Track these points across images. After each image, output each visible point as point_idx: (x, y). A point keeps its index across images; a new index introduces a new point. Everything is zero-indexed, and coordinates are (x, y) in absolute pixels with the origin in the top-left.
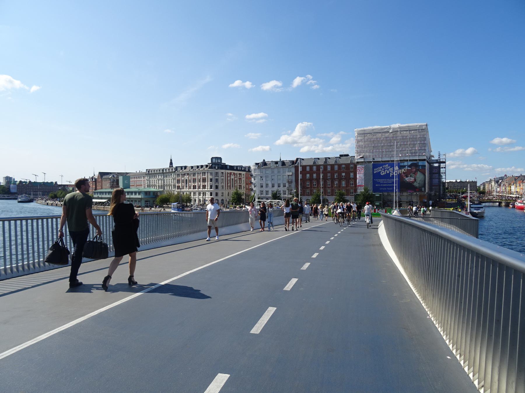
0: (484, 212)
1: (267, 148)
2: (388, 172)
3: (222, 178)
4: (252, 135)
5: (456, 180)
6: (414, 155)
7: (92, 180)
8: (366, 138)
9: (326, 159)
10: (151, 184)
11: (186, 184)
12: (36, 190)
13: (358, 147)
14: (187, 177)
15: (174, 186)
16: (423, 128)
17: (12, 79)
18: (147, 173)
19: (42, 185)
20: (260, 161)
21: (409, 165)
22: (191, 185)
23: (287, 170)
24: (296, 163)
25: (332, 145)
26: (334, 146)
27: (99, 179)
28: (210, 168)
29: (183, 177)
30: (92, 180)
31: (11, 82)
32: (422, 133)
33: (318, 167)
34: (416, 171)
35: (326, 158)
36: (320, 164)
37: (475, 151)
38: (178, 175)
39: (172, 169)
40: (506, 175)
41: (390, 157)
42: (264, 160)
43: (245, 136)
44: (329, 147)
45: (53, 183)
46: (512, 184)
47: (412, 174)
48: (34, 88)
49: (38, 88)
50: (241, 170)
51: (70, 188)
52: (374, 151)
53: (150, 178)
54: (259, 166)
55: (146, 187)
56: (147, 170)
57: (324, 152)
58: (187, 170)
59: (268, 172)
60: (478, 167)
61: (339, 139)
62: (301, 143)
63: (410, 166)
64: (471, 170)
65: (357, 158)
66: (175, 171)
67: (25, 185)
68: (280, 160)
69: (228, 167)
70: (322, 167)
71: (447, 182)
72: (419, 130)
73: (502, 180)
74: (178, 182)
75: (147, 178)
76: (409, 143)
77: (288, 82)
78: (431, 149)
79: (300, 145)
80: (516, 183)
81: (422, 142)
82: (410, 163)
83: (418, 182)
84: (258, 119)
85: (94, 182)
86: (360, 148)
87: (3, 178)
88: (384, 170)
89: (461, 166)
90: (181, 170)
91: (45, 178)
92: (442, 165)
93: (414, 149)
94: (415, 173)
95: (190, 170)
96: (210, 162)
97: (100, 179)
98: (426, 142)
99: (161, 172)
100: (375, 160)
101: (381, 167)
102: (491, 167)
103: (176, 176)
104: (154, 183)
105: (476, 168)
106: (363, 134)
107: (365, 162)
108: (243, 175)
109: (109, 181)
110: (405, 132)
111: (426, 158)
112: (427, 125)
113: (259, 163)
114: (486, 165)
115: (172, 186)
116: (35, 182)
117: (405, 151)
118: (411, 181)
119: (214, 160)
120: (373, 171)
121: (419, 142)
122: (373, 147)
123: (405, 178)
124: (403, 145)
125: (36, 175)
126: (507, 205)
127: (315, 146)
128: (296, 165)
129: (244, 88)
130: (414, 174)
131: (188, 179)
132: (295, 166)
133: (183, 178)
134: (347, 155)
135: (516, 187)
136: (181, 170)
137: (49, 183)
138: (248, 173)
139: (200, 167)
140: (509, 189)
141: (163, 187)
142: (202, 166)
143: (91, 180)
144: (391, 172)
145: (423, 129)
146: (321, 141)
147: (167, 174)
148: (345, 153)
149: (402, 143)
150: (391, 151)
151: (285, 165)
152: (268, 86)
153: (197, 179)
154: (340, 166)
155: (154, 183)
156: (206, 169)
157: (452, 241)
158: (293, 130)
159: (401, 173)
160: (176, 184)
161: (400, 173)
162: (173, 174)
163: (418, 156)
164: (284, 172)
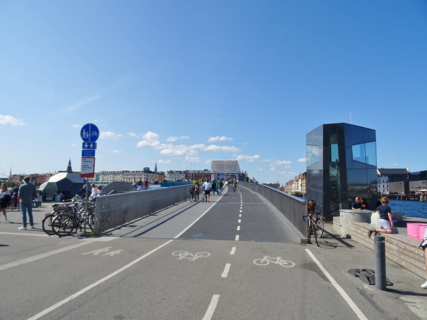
3: (150, 177)
6: (232, 171)
10: (115, 179)
11: (129, 179)
13: (212, 167)
18: (102, 173)
20: (169, 170)
23: (182, 175)
28: (144, 172)
33: (196, 174)
34: (233, 178)
35: (199, 171)
36: (196, 173)
42: (171, 170)
65: (212, 172)
66: (122, 173)
69: (152, 173)
70: (197, 174)
82: (231, 174)
103: (123, 175)
110: (229, 163)
119: (146, 169)
121: (234, 167)
128: (186, 173)
131: (130, 177)
134: (207, 170)
139: (138, 172)
142: (139, 172)
148: (207, 169)
153: (136, 177)
154: (204, 174)
164: (181, 176)
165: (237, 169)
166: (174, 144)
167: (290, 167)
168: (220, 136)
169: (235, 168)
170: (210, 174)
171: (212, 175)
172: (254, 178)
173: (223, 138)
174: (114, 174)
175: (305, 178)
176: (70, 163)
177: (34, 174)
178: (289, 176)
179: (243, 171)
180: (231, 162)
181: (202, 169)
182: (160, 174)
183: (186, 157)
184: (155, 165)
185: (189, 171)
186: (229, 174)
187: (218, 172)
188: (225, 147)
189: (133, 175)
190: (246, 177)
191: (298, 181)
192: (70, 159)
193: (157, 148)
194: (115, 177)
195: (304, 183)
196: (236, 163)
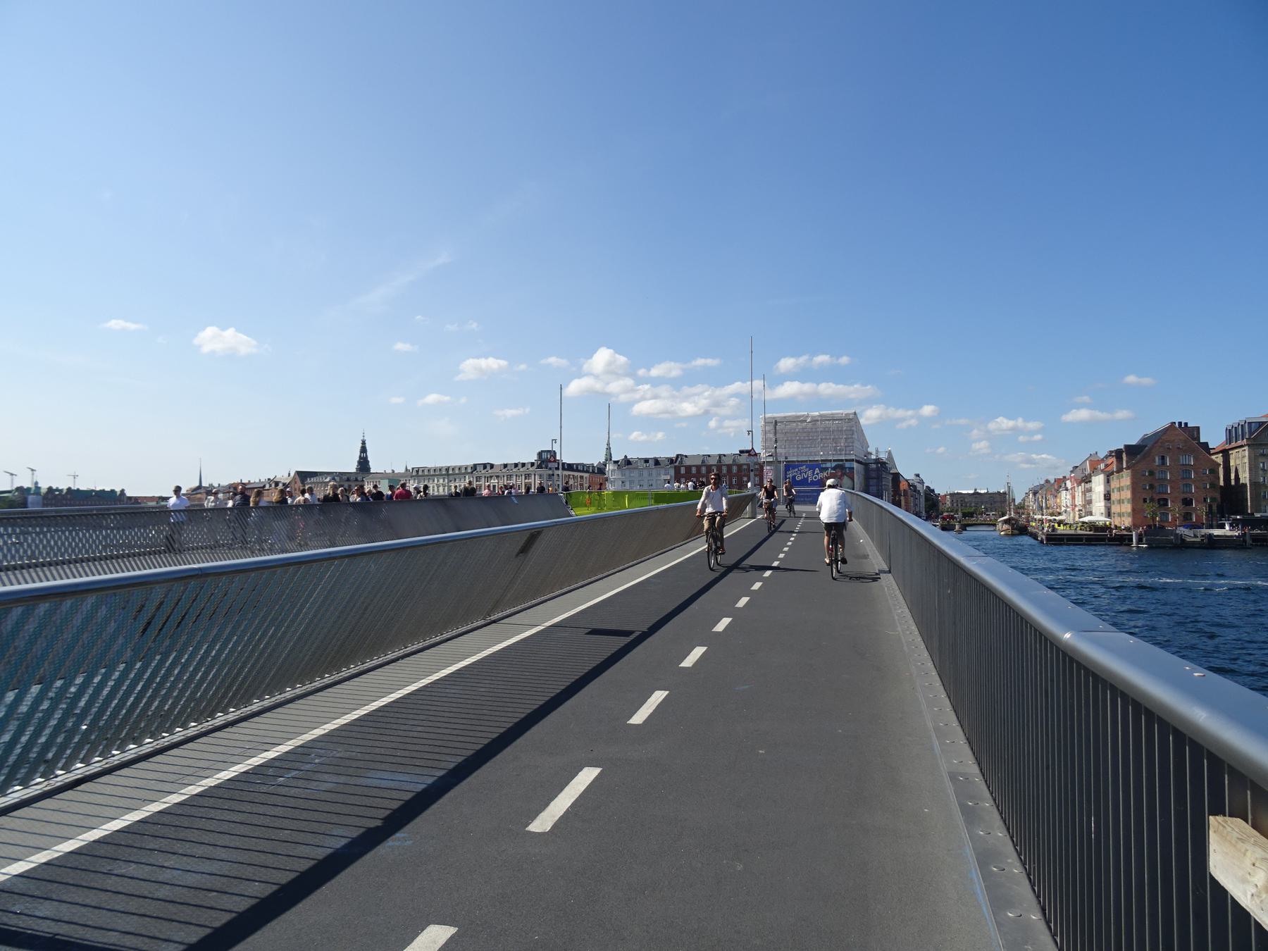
2: (806, 477)
5: (976, 490)
6: (839, 453)
9: (720, 457)
18: (414, 473)
23: (663, 471)
24: (676, 462)
27: (296, 483)
28: (538, 467)
33: (709, 469)
34: (843, 475)
35: (720, 456)
42: (626, 456)
48: (463, 400)
50: (583, 471)
52: (787, 446)
66: (472, 472)
67: (59, 497)
82: (834, 464)
88: (801, 474)
99: (463, 471)
100: (788, 460)
101: (796, 470)
110: (827, 422)
119: (544, 456)
128: (677, 464)
132: (675, 467)
139: (520, 466)
142: (523, 465)
143: (273, 485)
149: (824, 437)
154: (740, 466)
157: (1128, 696)
162: (467, 477)
165: (857, 444)
166: (676, 384)
167: (1038, 437)
168: (815, 354)
169: (849, 441)
170: (760, 464)
171: (766, 468)
172: (918, 475)
173: (822, 359)
174: (448, 475)
175: (1128, 468)
176: (364, 450)
177: (238, 484)
178: (1033, 466)
179: (877, 451)
180: (833, 418)
181: (730, 448)
182: (593, 472)
183: (712, 419)
184: (606, 446)
185: (686, 456)
186: (828, 465)
187: (786, 458)
188: (831, 384)
189: (523, 477)
190: (891, 472)
191: (1087, 480)
192: (365, 438)
193: (623, 398)
194: (451, 486)
195: (1120, 489)
196: (853, 423)
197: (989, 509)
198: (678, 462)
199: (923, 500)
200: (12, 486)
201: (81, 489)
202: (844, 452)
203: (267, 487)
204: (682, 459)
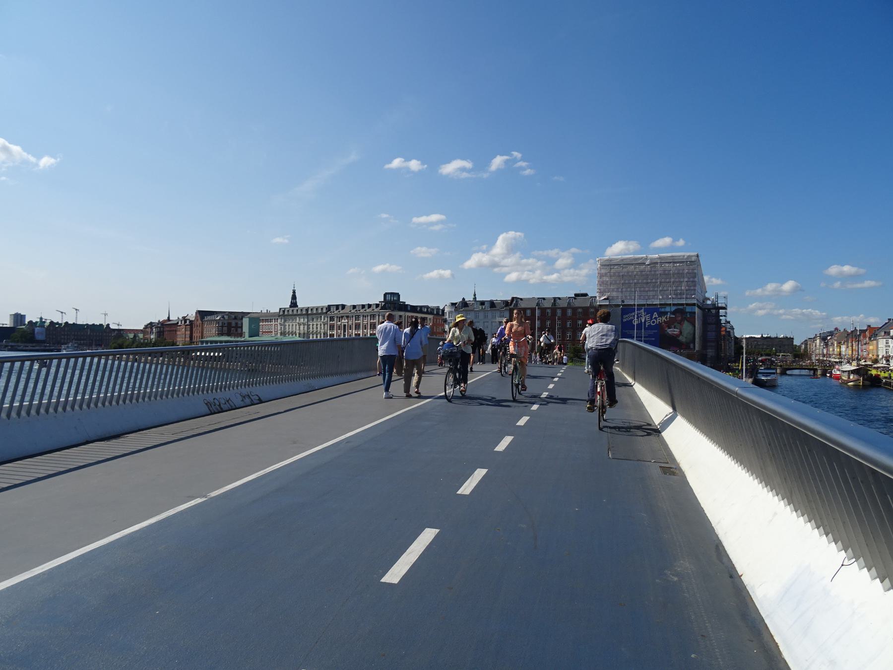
0: (775, 380)
1: (447, 273)
4: (422, 252)
5: (762, 335)
6: (679, 296)
7: (185, 322)
8: (612, 271)
9: (555, 301)
11: (345, 331)
12: (85, 337)
13: (601, 283)
14: (346, 321)
15: (324, 334)
16: (693, 260)
17: (7, 144)
18: (281, 313)
19: (85, 329)
20: (458, 300)
21: (672, 311)
22: (352, 333)
23: (498, 314)
24: (511, 305)
25: (558, 271)
26: (560, 274)
27: (197, 321)
29: (339, 322)
30: (185, 322)
31: (5, 149)
32: (691, 266)
33: (543, 310)
35: (555, 299)
37: (797, 287)
38: (332, 319)
39: (297, 310)
40: (836, 329)
41: (647, 299)
42: (464, 299)
43: (412, 252)
44: (553, 274)
45: (103, 326)
46: (843, 342)
47: (676, 324)
49: (52, 161)
50: (427, 313)
51: (129, 335)
52: (624, 290)
53: (285, 321)
54: (456, 307)
55: (279, 334)
56: (280, 309)
57: (544, 283)
58: (346, 310)
59: (470, 316)
60: (803, 314)
61: (569, 261)
62: (506, 266)
63: (673, 313)
64: (792, 318)
65: (600, 300)
66: (326, 313)
67: (59, 329)
68: (475, 298)
69: (409, 309)
70: (549, 311)
71: (746, 338)
72: (687, 262)
73: (832, 336)
74: (331, 329)
75: (281, 321)
76: (672, 280)
77: (481, 163)
78: (706, 289)
79: (506, 269)
80: (847, 341)
81: (691, 279)
82: (673, 308)
83: (685, 336)
84: (432, 224)
85: (189, 327)
86: (603, 287)
87: (9, 316)
89: (775, 312)
90: (336, 310)
91: (76, 318)
92: (722, 312)
93: (680, 288)
94: (681, 323)
95: (350, 311)
96: (383, 300)
97: (200, 321)
98: (696, 279)
99: (320, 311)
100: (625, 303)
102: (824, 314)
104: (317, 328)
105: (799, 316)
106: (608, 265)
107: (611, 305)
108: (430, 319)
109: (216, 325)
110: (667, 265)
111: (696, 302)
112: (698, 256)
113: (456, 303)
114: (817, 311)
115: (321, 334)
116: (74, 323)
117: (667, 292)
118: (674, 334)
119: (388, 297)
120: (622, 318)
121: (686, 279)
122: (622, 284)
123: (666, 329)
124: (664, 282)
125: (62, 313)
126: (824, 374)
127: (528, 272)
129: (408, 170)
130: (679, 325)
131: (347, 324)
132: (510, 309)
133: (340, 323)
134: (586, 295)
135: (848, 347)
136: (336, 310)
137: (97, 325)
138: (436, 317)
140: (838, 350)
141: (306, 335)
142: (370, 306)
143: (183, 322)
144: (647, 320)
145: (692, 261)
146: (539, 263)
147: (314, 316)
150: (647, 291)
151: (496, 307)
152: (451, 168)
154: (574, 309)
155: (317, 328)
156: (376, 310)
158: (493, 243)
159: (661, 322)
160: (328, 331)
161: (659, 322)
162: (323, 317)
163: (671, 300)
186: (668, 309)
187: (623, 301)
196: (696, 266)
197: (778, 351)
198: (513, 305)
199: (733, 343)
200: (62, 321)
201: (95, 324)
202: (684, 296)
203: (180, 324)
204: (517, 301)
